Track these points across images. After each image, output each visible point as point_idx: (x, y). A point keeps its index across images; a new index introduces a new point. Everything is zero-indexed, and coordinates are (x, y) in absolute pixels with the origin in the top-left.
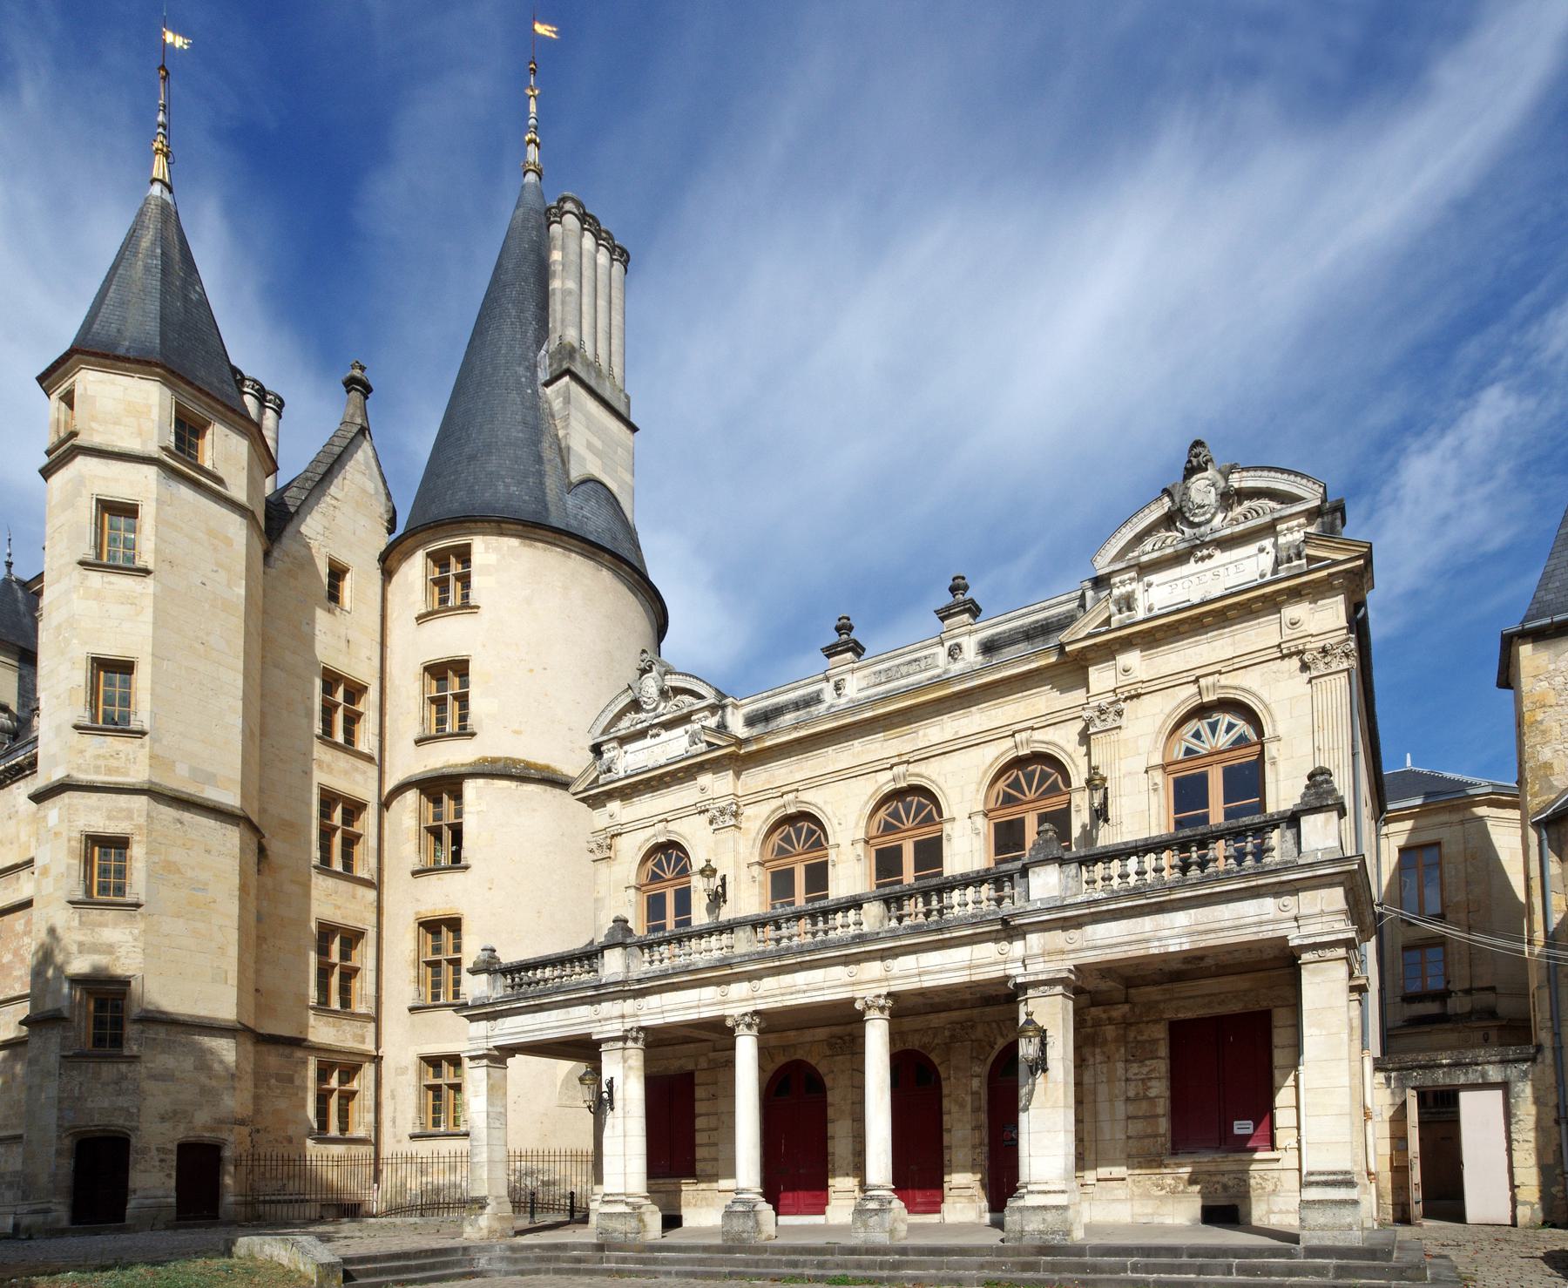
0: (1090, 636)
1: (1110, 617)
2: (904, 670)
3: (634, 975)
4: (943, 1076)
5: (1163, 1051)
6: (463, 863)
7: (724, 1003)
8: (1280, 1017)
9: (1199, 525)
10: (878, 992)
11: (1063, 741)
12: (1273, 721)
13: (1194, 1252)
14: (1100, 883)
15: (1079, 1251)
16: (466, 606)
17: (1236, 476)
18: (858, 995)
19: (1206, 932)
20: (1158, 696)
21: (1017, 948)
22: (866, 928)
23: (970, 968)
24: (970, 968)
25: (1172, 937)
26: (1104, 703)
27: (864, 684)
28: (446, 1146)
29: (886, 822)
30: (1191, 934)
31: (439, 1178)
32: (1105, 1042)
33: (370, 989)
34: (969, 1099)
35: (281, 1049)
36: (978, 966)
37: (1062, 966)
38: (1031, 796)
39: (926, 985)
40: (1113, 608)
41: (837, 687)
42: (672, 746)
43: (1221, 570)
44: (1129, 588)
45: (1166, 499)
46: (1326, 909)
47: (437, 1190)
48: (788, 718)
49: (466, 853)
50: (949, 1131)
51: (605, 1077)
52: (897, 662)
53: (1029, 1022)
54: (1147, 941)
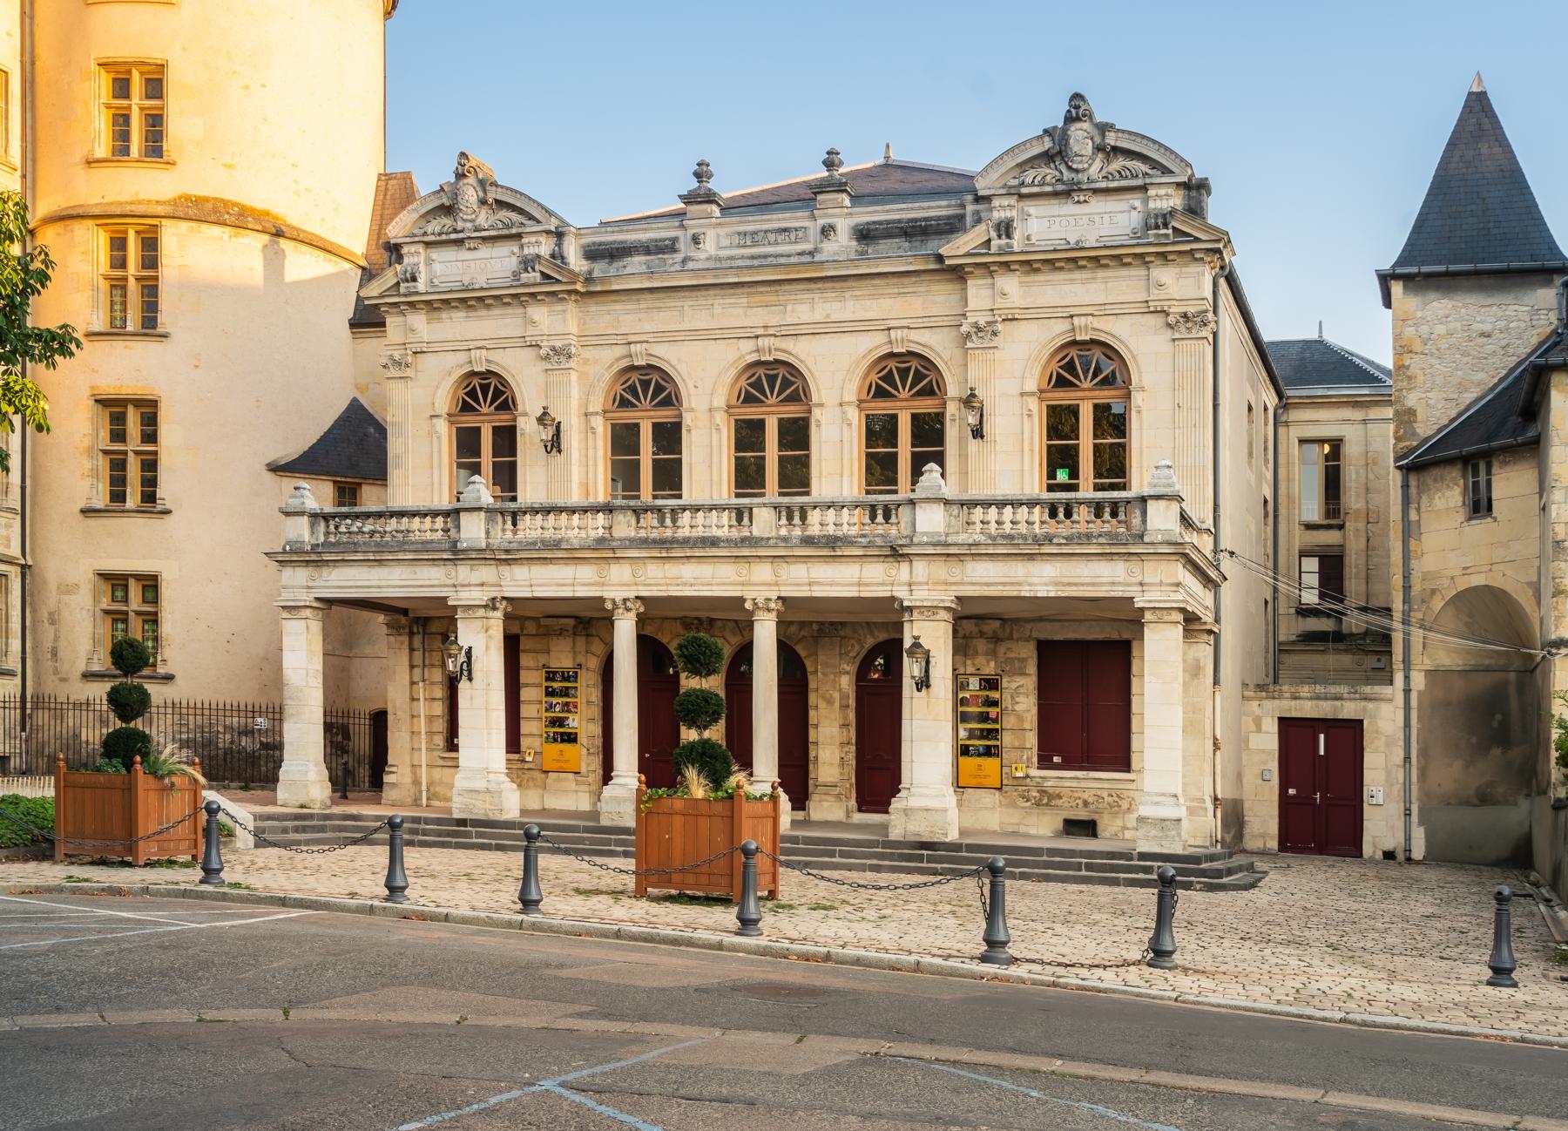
1: (989, 241)
2: (772, 237)
4: (810, 669)
5: (1032, 668)
6: (160, 330)
8: (1135, 645)
9: (1077, 171)
10: (768, 595)
11: (937, 345)
12: (1140, 372)
13: (1052, 852)
14: (979, 526)
15: (956, 847)
19: (1070, 584)
22: (756, 533)
26: (982, 323)
27: (726, 242)
29: (747, 392)
30: (1056, 584)
32: (976, 653)
34: (837, 696)
36: (867, 585)
37: (947, 597)
38: (904, 394)
40: (993, 234)
41: (696, 240)
44: (1008, 214)
45: (1047, 139)
48: (637, 263)
50: (816, 726)
53: (916, 645)
54: (1019, 584)
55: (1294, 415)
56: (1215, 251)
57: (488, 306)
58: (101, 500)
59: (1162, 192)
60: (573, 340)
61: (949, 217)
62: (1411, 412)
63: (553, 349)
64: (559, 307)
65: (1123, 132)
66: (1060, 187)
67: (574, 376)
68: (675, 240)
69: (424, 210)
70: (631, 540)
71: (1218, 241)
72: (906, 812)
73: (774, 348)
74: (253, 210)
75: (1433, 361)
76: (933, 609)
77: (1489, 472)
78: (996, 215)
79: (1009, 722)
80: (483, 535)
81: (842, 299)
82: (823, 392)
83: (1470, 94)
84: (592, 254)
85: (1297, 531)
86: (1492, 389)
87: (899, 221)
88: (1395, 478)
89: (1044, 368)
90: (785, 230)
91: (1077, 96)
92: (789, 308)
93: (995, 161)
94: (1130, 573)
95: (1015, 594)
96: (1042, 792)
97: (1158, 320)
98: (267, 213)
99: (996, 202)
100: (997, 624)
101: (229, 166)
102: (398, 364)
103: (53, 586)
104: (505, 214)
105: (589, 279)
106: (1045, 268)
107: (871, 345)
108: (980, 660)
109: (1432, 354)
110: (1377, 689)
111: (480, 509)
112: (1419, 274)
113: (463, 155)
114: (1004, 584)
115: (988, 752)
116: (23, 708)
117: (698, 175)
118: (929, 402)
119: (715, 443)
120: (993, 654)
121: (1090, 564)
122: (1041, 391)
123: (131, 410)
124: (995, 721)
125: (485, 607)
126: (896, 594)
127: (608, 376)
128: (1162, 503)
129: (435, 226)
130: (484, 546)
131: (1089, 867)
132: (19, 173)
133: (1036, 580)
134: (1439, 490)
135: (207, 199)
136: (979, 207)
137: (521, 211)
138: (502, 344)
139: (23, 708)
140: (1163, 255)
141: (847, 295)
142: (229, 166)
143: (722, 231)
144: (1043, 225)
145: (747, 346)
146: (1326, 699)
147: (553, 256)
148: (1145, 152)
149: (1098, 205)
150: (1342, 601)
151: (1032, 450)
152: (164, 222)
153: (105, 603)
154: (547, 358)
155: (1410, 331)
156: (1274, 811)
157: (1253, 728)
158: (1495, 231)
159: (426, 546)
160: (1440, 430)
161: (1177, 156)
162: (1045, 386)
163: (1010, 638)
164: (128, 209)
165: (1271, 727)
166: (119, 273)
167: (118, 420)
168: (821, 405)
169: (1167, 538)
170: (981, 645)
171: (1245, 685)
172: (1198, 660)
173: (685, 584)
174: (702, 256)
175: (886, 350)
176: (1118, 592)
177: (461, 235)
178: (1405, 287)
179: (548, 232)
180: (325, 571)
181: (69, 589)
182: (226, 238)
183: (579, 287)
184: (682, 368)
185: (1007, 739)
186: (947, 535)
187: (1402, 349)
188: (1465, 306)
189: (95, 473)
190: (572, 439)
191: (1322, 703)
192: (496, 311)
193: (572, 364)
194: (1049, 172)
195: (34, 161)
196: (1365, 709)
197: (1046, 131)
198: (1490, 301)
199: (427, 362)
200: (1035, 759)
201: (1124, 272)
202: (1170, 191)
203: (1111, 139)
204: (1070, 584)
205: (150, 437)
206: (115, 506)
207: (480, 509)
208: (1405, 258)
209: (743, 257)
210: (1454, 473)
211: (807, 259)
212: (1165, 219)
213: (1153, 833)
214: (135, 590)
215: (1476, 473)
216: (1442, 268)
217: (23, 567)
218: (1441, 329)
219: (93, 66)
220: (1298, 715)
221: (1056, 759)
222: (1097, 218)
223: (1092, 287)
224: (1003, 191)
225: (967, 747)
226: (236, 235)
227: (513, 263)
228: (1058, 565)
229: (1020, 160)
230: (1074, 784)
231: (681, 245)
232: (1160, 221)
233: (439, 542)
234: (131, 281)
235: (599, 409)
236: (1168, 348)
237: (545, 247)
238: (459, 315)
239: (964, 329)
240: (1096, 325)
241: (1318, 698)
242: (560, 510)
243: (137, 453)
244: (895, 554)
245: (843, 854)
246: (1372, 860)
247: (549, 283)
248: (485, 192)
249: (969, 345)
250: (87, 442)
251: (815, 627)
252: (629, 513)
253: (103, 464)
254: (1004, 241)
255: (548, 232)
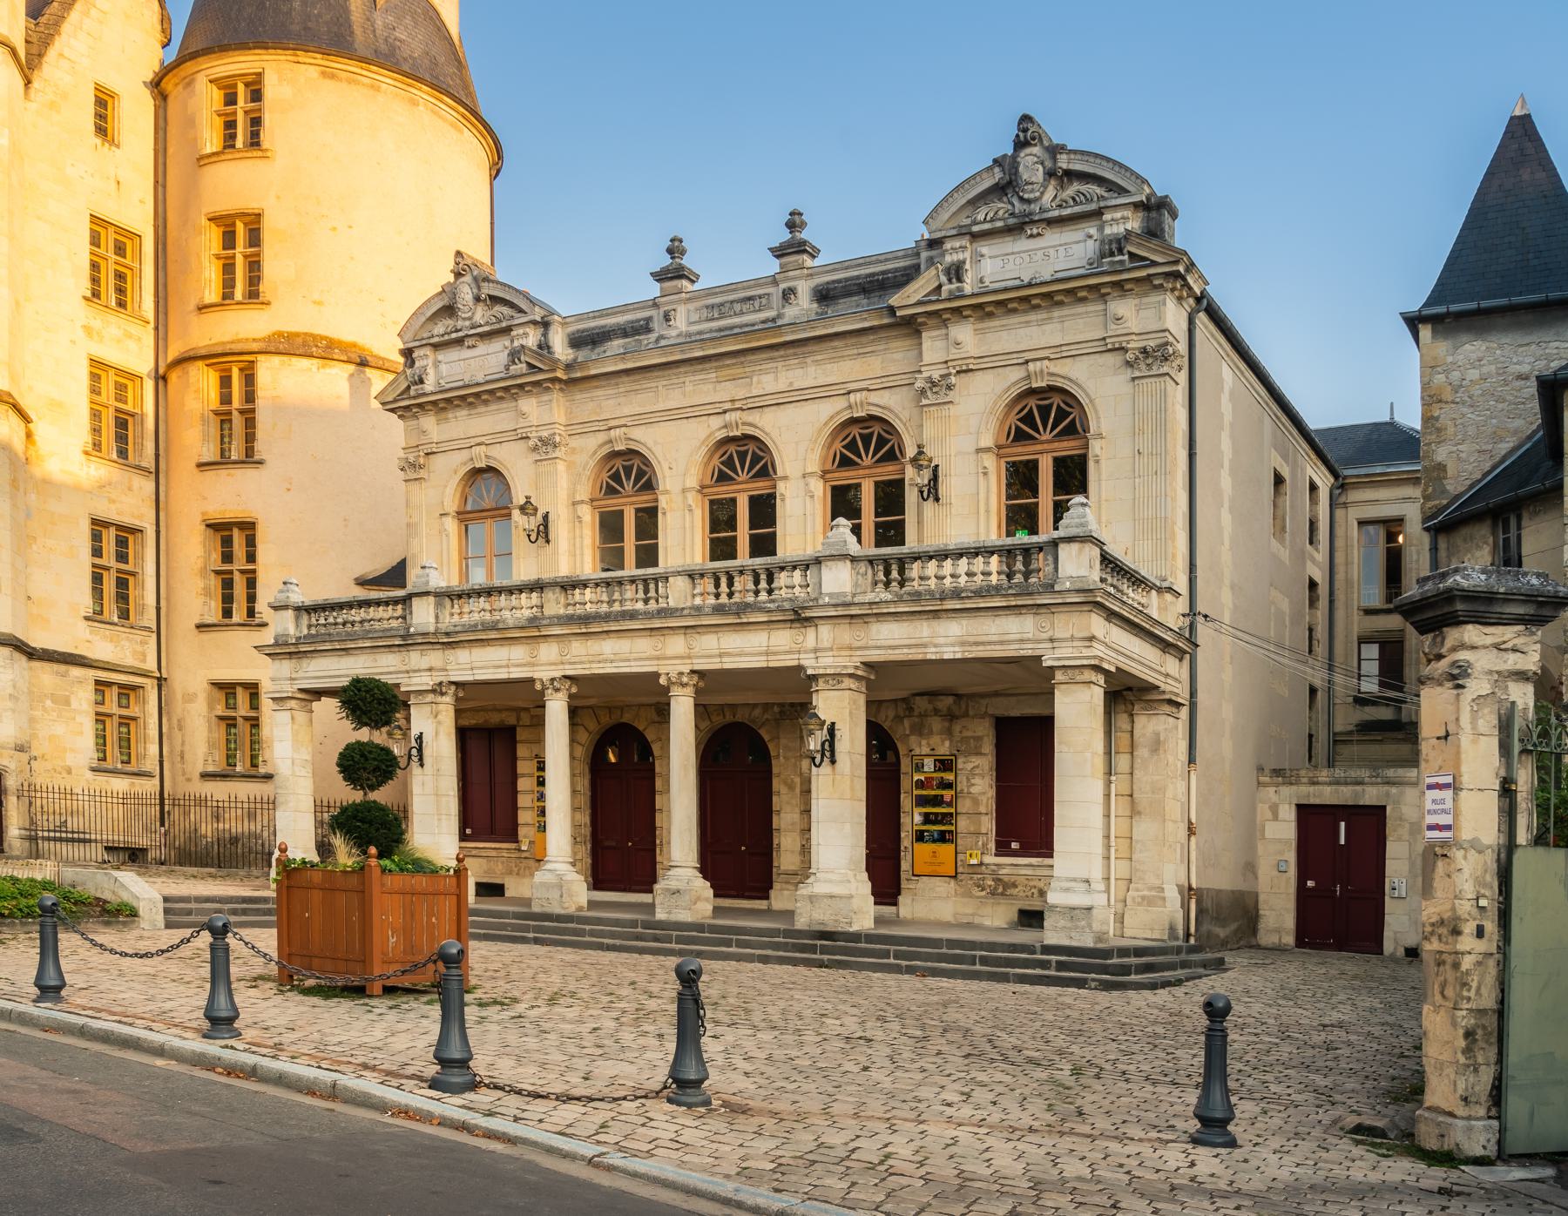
0: (920, 303)
1: (940, 286)
2: (737, 307)
3: (443, 627)
5: (988, 747)
6: (256, 458)
7: (534, 665)
9: (1029, 201)
11: (894, 405)
16: (250, 458)
17: (1064, 156)
18: (662, 670)
19: (977, 644)
20: (988, 377)
21: (810, 637)
22: (672, 604)
23: (767, 654)
24: (767, 654)
25: (946, 645)
26: (936, 376)
27: (695, 317)
28: (245, 790)
30: (963, 644)
31: (235, 825)
32: (931, 733)
33: (150, 599)
34: (797, 780)
35: (55, 666)
36: (775, 653)
37: (849, 662)
39: (726, 666)
40: (944, 279)
41: (667, 318)
42: (486, 362)
43: (1052, 252)
44: (961, 256)
45: (997, 170)
46: (1077, 635)
47: (234, 840)
48: (616, 345)
49: (260, 446)
51: (414, 732)
52: (731, 297)
54: (925, 646)
55: (1354, 496)
56: (1176, 275)
57: (486, 402)
58: (213, 614)
59: (1118, 215)
60: (560, 429)
61: (905, 268)
62: (1441, 467)
63: (540, 439)
64: (546, 398)
65: (1075, 152)
66: (1012, 221)
67: (561, 466)
68: (649, 319)
69: (429, 314)
70: (559, 617)
71: (1176, 262)
72: (812, 898)
73: (741, 424)
74: (340, 342)
75: (1465, 410)
76: (838, 677)
77: (1519, 528)
78: (948, 259)
79: (964, 805)
80: (432, 620)
81: (803, 365)
82: (787, 465)
83: (1512, 118)
84: (576, 342)
85: (1356, 616)
86: (1529, 437)
87: (858, 277)
88: (1426, 539)
89: (1002, 423)
90: (750, 299)
91: (1026, 118)
92: (755, 379)
93: (945, 199)
94: (1041, 629)
95: (920, 657)
96: (998, 880)
97: (1113, 360)
98: (355, 345)
99: (948, 245)
100: (950, 700)
101: (318, 303)
102: (413, 466)
103: (179, 697)
104: (499, 309)
105: (569, 367)
106: (998, 311)
107: (828, 412)
108: (935, 740)
109: (1464, 403)
110: (1400, 772)
111: (427, 593)
112: (1448, 314)
113: (459, 254)
114: (909, 646)
115: (943, 838)
116: (162, 804)
117: (670, 251)
118: (891, 468)
119: (688, 525)
120: (949, 733)
121: (998, 621)
122: (999, 447)
123: (236, 532)
124: (950, 804)
125: (433, 691)
126: (803, 662)
127: (592, 463)
128: (1075, 547)
129: (439, 328)
130: (432, 629)
131: (984, 961)
132: (152, 325)
133: (942, 640)
134: (1468, 551)
135: (297, 335)
136: (933, 253)
137: (512, 305)
138: (498, 438)
139: (162, 804)
140: (1118, 285)
141: (809, 360)
142: (318, 303)
143: (691, 306)
144: (996, 265)
145: (716, 422)
146: (1346, 784)
147: (540, 347)
148: (1100, 172)
149: (1053, 237)
150: (1400, 689)
151: (987, 511)
152: (260, 358)
153: (220, 710)
154: (535, 449)
155: (1440, 379)
156: (1291, 904)
157: (1269, 815)
158: (1535, 262)
159: (387, 634)
160: (1471, 486)
161: (1133, 173)
162: (1003, 441)
163: (966, 715)
164: (227, 348)
165: (1289, 814)
166: (225, 408)
167: (227, 542)
168: (785, 478)
169: (1079, 586)
170: (936, 724)
171: (1260, 769)
172: (1158, 734)
173: (605, 661)
174: (674, 333)
175: (846, 416)
176: (1027, 650)
177: (460, 334)
178: (1434, 331)
179: (534, 323)
180: (305, 662)
181: (189, 698)
182: (314, 369)
183: (560, 374)
184: (658, 450)
185: (963, 824)
186: (854, 595)
187: (1431, 399)
188: (1501, 347)
189: (207, 592)
190: (561, 530)
191: (1342, 788)
192: (493, 407)
193: (557, 453)
194: (1000, 207)
195: (166, 314)
196: (1388, 794)
197: (995, 161)
198: (1527, 339)
199: (438, 462)
200: (992, 846)
201: (1080, 309)
202: (1128, 213)
203: (1063, 162)
204: (977, 644)
205: (251, 558)
206: (227, 621)
207: (427, 593)
208: (1435, 298)
209: (711, 331)
210: (1483, 531)
211: (770, 325)
212: (1116, 245)
213: (1062, 923)
214: (242, 697)
215: (1506, 530)
216: (1472, 305)
217: (159, 679)
218: (1474, 374)
219: (204, 222)
220: (1318, 802)
221: (1014, 845)
222: (1052, 252)
223: (1048, 328)
224: (954, 232)
225: (922, 832)
226: (323, 366)
227: (503, 357)
228: (964, 622)
229: (970, 196)
230: (1029, 872)
231: (655, 325)
232: (1114, 246)
233: (397, 629)
234: (235, 413)
235: (586, 497)
236: (1127, 388)
237: (532, 338)
238: (462, 413)
239: (919, 384)
240: (1053, 369)
241: (1338, 783)
242: (500, 591)
243: (242, 572)
244: (799, 617)
245: (740, 944)
246: (1393, 958)
247: (535, 376)
248: (479, 288)
249: (925, 402)
250: (200, 563)
251: (776, 709)
252: (558, 589)
253: (215, 583)
254: (955, 285)
255: (534, 323)
